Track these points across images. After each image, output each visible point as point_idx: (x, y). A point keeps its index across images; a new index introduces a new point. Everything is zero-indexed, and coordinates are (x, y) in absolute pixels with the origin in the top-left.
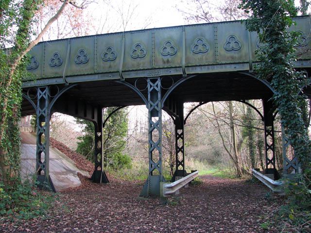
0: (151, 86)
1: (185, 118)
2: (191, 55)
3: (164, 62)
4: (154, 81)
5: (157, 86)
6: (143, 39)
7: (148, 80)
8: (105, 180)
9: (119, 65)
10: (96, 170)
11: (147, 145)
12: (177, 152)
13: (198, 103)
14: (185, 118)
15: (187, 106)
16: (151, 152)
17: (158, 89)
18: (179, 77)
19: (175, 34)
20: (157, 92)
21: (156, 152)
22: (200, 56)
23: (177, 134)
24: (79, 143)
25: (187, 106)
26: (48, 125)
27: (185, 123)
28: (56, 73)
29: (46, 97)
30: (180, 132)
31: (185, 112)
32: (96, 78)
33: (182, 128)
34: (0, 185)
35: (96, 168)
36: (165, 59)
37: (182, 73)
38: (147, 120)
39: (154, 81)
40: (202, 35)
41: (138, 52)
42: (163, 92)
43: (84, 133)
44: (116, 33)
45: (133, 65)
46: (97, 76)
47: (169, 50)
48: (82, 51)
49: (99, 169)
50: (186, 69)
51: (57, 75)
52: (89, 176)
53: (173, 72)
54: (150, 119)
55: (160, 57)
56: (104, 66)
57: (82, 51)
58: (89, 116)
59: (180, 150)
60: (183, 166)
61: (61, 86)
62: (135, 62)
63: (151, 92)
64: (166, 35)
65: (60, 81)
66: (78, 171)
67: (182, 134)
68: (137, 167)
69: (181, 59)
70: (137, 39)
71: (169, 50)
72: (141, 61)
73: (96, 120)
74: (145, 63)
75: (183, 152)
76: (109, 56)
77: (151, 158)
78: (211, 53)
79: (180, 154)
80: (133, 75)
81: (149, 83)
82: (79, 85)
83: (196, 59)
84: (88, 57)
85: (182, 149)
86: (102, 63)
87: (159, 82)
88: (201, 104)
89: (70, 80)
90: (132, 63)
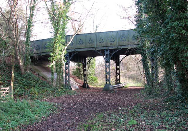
0: (106, 53)
1: (120, 62)
2: (120, 41)
3: (110, 44)
4: (107, 51)
5: (108, 52)
6: (103, 35)
7: (105, 51)
8: (88, 87)
9: (94, 45)
10: (84, 83)
11: (105, 73)
12: (117, 75)
13: (126, 55)
14: (120, 62)
15: (121, 57)
16: (106, 76)
17: (109, 54)
18: (115, 50)
19: (114, 34)
20: (108, 55)
21: (108, 75)
22: (123, 42)
23: (117, 68)
24: (73, 72)
25: (121, 57)
26: (69, 66)
27: (120, 64)
28: (71, 48)
29: (68, 56)
30: (118, 67)
31: (120, 59)
32: (86, 50)
33: (119, 66)
34: (187, 66)
35: (84, 82)
36: (111, 43)
37: (116, 48)
38: (105, 65)
39: (107, 51)
40: (124, 34)
41: (101, 40)
42: (110, 55)
43: (76, 67)
44: (113, 31)
45: (99, 45)
46: (86, 49)
47: (112, 39)
48: (81, 40)
49: (85, 82)
50: (118, 47)
51: (72, 48)
52: (81, 86)
53: (114, 48)
54: (106, 64)
55: (109, 42)
56: (89, 45)
57: (81, 40)
58: (82, 61)
59: (118, 74)
60: (119, 81)
61: (74, 52)
62: (100, 44)
63: (106, 55)
64: (111, 34)
65: (73, 50)
66: (77, 83)
67: (119, 68)
68: (100, 82)
69: (116, 43)
70: (101, 35)
71: (112, 39)
72: (103, 43)
73: (84, 63)
74: (104, 44)
75: (119, 75)
76: (91, 41)
77: (106, 78)
78: (127, 41)
79: (118, 76)
80: (100, 49)
81: (105, 52)
82: (80, 52)
83: (121, 43)
84: (83, 42)
85: (119, 74)
86: (88, 44)
87: (109, 51)
88: (127, 56)
89: (77, 50)
90: (99, 44)
